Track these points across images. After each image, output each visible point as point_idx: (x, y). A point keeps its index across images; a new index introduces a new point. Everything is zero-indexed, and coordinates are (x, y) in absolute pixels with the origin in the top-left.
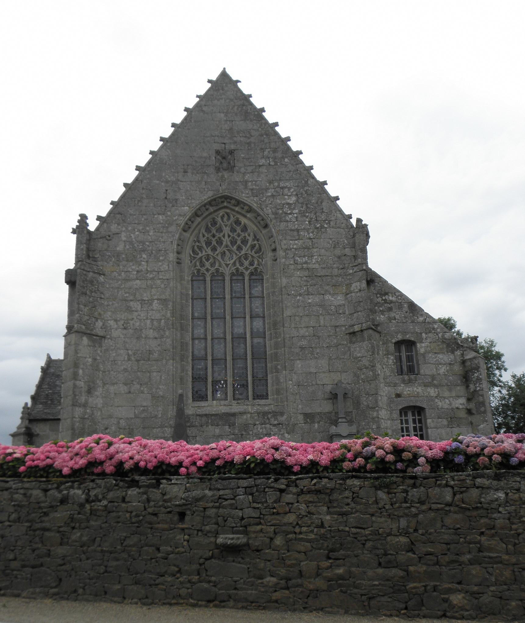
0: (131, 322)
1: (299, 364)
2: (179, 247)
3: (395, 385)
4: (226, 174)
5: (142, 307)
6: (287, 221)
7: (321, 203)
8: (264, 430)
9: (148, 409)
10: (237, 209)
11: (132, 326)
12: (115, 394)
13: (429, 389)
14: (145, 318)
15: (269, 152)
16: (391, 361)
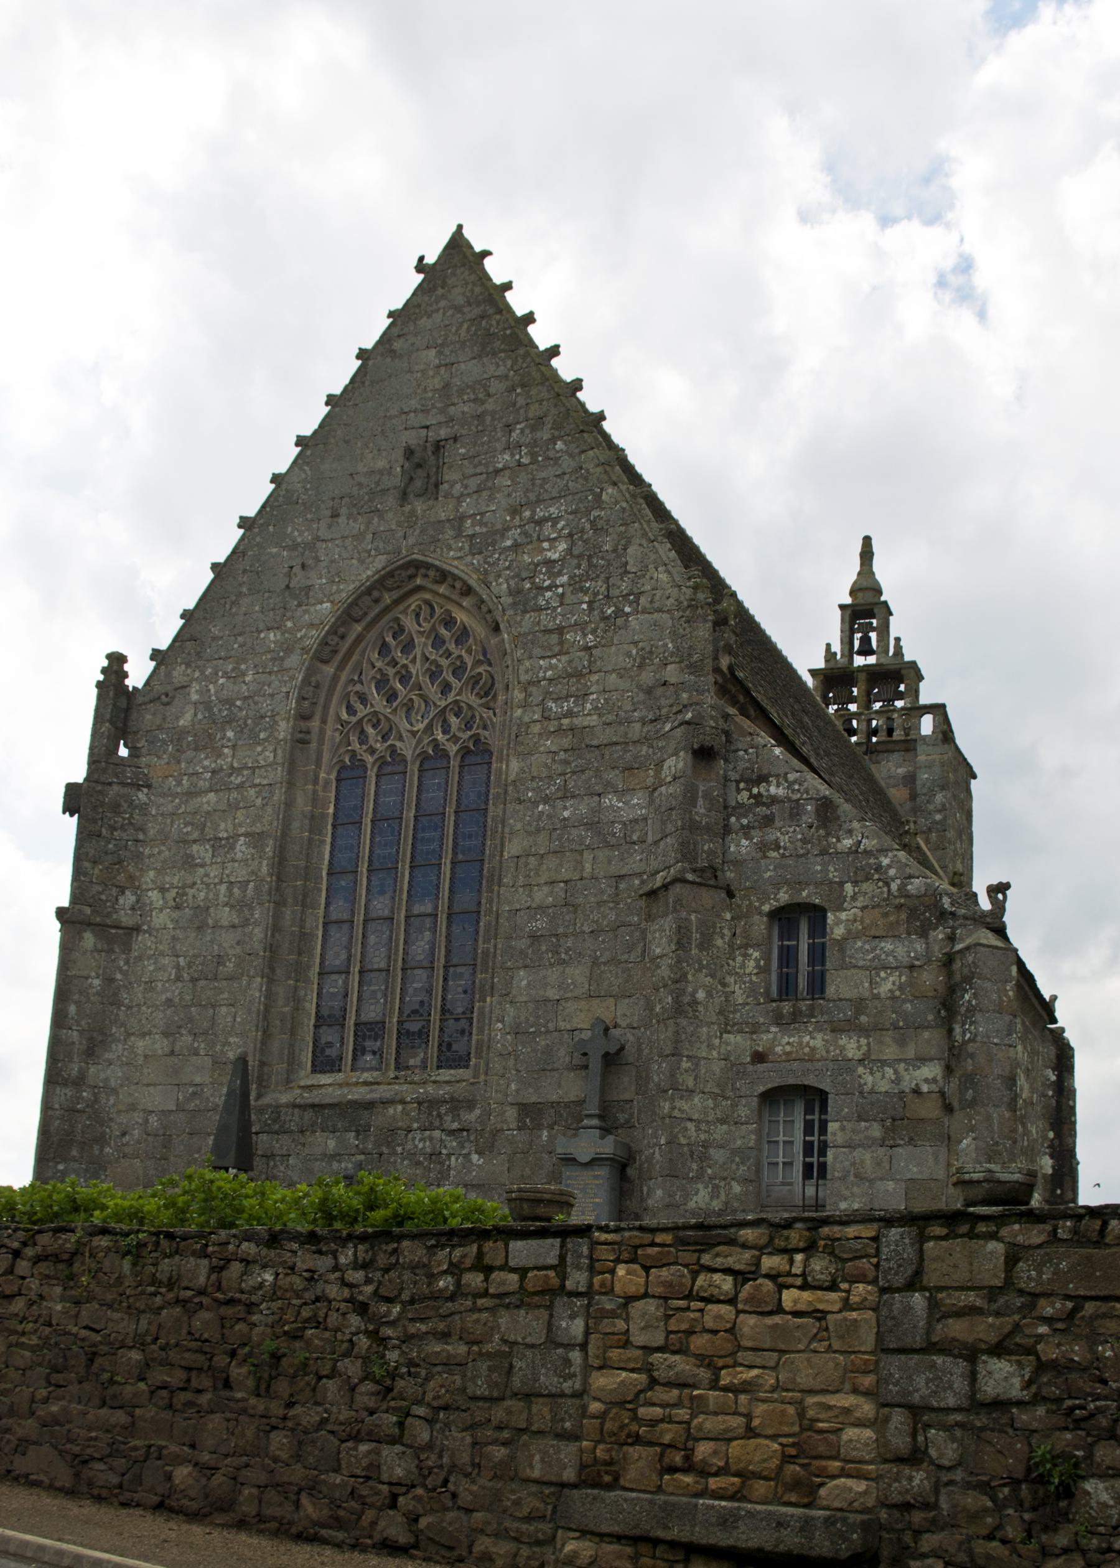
0: (191, 892)
1: (522, 979)
2: (306, 704)
3: (755, 1029)
4: (419, 506)
5: (213, 856)
6: (540, 609)
7: (625, 549)
8: (428, 1143)
9: (202, 1090)
10: (442, 589)
11: (190, 901)
12: (146, 1056)
13: (843, 1041)
14: (217, 880)
15: (522, 431)
16: (752, 964)
